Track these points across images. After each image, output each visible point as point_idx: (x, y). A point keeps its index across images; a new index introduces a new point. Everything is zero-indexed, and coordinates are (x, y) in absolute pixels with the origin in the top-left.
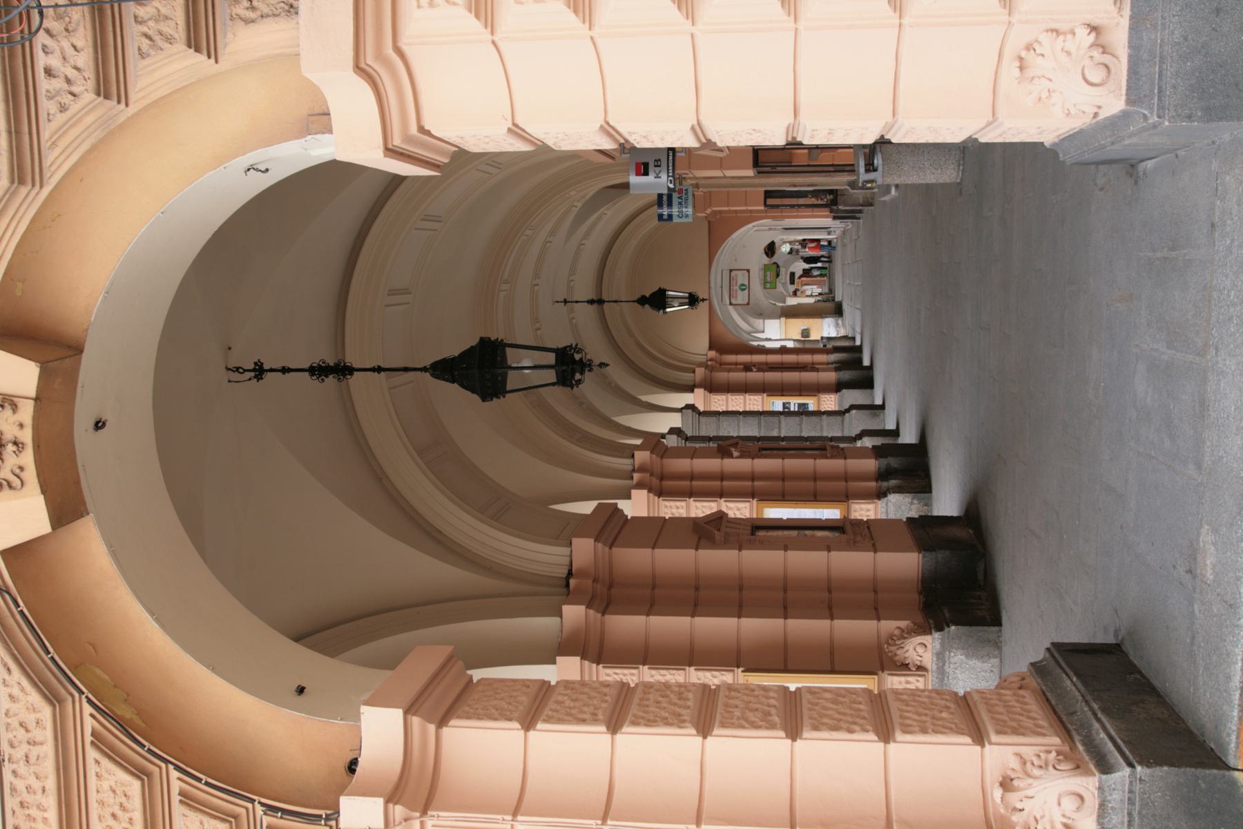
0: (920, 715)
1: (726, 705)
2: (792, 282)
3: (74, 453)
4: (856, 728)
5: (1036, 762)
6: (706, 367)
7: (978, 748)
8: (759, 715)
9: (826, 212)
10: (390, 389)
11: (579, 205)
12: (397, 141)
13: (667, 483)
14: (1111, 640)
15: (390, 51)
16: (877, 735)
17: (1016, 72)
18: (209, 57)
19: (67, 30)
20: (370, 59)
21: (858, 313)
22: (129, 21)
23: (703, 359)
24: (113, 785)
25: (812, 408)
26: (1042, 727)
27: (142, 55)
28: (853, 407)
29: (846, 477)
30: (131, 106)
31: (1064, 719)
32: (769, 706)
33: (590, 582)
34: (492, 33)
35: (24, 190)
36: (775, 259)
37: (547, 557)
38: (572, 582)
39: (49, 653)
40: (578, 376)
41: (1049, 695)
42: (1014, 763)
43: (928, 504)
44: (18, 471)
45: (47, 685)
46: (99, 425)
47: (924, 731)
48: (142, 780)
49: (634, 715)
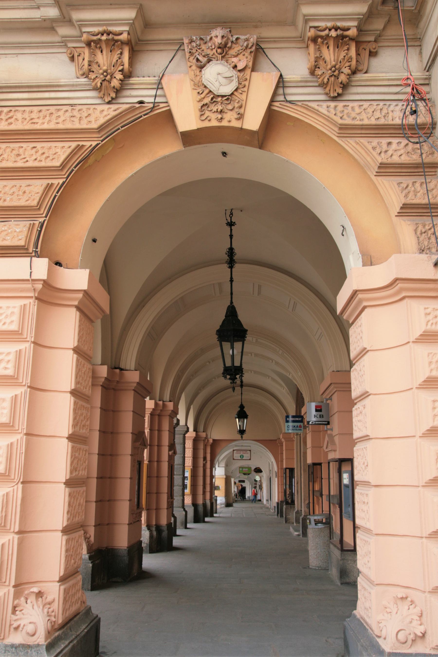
0: (73, 548)
1: (80, 449)
2: (240, 481)
3: (214, 143)
4: (69, 516)
5: (51, 610)
6: (206, 438)
7: (58, 579)
8: (76, 466)
9: (282, 498)
10: (214, 284)
11: (290, 377)
12: (360, 296)
13: (157, 418)
14: (101, 650)
15: (403, 294)
16: (66, 526)
17: (400, 596)
18: (398, 213)
19: (408, 153)
20: (400, 285)
21: (229, 515)
22: (413, 179)
23: (209, 437)
24: (58, 154)
25: (186, 491)
26: (66, 613)
27: (399, 184)
28: (186, 512)
29: (158, 509)
30: (375, 177)
31: (68, 625)
32: (79, 470)
33: (118, 379)
34: (413, 342)
35: (336, 129)
36: (253, 473)
37: (130, 359)
38: (118, 371)
39: (122, 128)
40: (228, 377)
41: (78, 617)
42: (50, 599)
43: (146, 553)
44: (209, 119)
45: (107, 126)
46: (224, 154)
47: (67, 551)
48: (60, 167)
49: (78, 403)
